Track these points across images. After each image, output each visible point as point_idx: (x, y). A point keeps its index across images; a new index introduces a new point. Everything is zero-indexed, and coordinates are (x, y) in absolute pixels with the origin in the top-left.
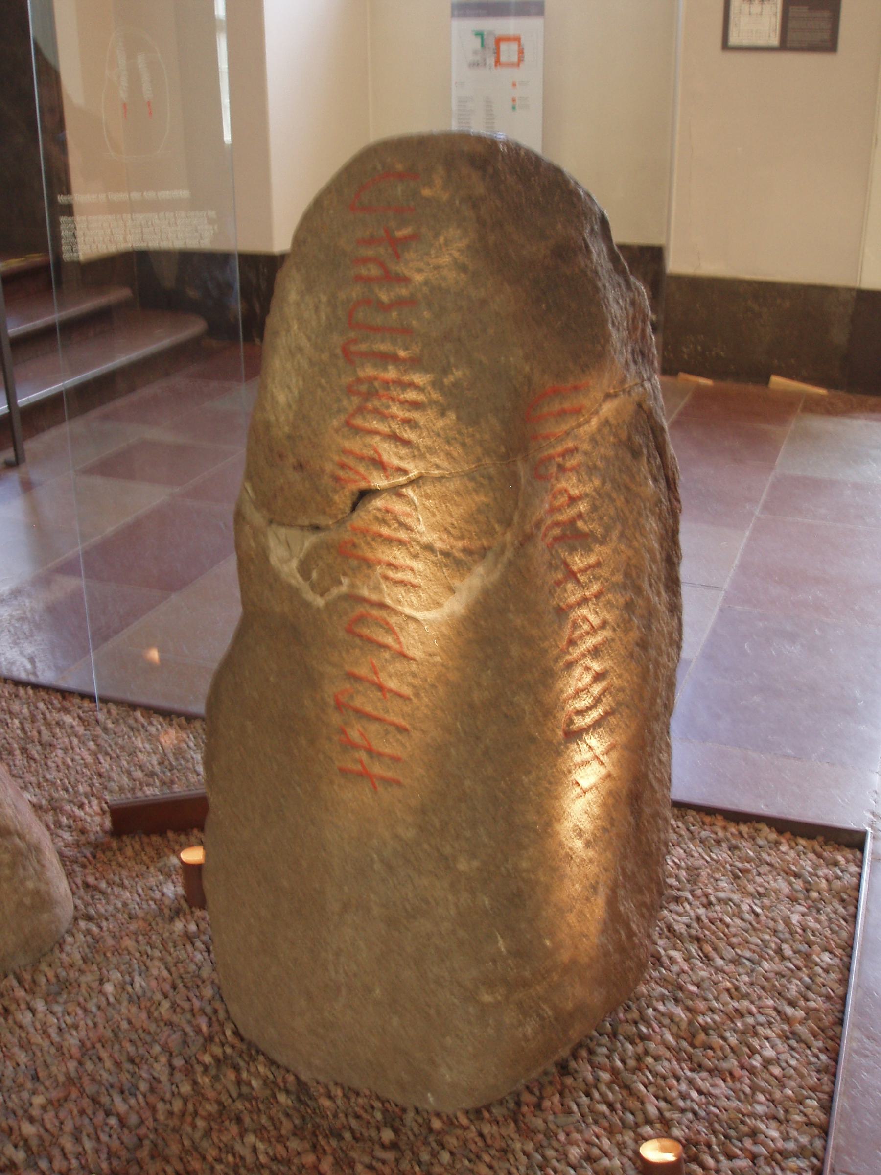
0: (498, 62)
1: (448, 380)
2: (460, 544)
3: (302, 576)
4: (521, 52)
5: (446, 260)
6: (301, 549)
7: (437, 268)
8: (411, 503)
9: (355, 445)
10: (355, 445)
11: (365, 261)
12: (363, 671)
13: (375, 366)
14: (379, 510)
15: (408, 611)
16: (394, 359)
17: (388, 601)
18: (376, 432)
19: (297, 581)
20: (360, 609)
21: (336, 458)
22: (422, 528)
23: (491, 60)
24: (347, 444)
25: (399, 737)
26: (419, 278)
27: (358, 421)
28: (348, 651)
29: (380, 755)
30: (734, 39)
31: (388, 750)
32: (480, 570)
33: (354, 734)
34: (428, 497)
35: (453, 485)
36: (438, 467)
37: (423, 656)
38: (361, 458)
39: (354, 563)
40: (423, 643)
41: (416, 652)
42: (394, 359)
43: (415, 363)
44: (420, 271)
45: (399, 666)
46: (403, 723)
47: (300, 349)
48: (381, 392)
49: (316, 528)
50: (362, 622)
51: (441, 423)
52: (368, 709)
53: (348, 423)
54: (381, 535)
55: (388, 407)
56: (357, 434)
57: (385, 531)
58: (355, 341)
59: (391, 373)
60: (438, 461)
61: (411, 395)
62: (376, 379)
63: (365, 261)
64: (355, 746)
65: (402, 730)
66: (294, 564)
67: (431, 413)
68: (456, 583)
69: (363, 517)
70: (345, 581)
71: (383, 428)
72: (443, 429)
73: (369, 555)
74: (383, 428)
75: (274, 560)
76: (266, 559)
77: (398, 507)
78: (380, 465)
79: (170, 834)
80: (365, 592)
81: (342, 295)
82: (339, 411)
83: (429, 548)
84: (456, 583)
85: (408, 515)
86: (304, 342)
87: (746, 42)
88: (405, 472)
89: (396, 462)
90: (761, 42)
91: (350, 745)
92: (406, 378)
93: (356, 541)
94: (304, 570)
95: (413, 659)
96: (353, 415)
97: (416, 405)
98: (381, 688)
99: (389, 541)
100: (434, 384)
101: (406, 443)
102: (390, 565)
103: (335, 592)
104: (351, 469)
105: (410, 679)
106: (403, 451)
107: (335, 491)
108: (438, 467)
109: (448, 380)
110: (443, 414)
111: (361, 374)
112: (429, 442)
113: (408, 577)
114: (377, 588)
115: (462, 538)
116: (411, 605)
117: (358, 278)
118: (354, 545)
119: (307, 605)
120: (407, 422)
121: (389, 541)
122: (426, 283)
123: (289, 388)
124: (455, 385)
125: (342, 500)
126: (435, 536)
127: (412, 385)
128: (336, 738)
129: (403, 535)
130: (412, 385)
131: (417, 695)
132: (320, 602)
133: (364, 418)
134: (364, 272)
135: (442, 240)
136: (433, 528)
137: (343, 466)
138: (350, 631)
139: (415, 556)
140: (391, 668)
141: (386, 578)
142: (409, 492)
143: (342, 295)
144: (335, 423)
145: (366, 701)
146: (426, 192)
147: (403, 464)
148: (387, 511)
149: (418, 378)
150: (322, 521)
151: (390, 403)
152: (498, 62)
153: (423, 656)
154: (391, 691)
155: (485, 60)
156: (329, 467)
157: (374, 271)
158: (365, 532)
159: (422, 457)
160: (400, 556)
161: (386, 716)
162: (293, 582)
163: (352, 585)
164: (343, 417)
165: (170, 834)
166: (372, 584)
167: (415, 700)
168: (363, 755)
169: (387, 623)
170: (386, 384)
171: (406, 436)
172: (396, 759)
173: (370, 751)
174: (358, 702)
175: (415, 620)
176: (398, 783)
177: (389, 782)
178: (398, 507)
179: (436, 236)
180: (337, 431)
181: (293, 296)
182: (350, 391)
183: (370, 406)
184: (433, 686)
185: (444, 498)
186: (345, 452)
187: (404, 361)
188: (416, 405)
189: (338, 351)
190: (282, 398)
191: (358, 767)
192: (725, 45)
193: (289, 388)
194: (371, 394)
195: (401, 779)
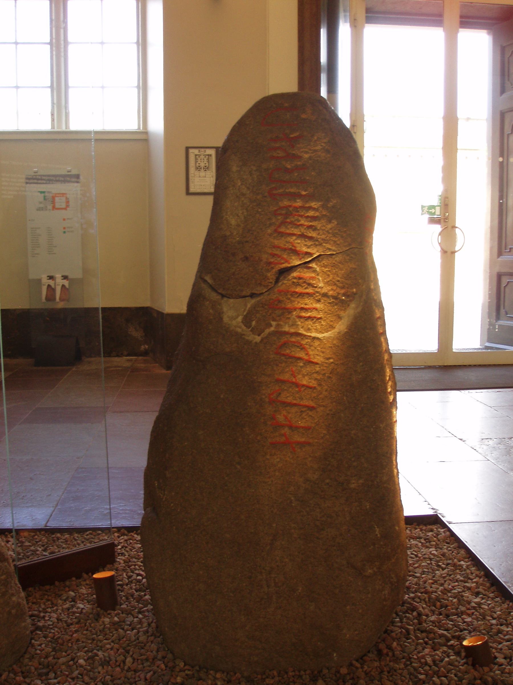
0: (54, 208)
1: (330, 204)
2: (343, 291)
3: (245, 326)
4: (68, 202)
5: (319, 148)
6: (245, 310)
7: (315, 151)
8: (315, 271)
9: (281, 242)
10: (281, 242)
11: (276, 149)
12: (286, 377)
13: (289, 200)
14: (295, 278)
15: (313, 335)
16: (300, 196)
17: (302, 331)
18: (293, 235)
19: (242, 329)
20: (284, 339)
21: (270, 251)
22: (321, 285)
23: (50, 207)
24: (276, 242)
25: (310, 413)
26: (306, 156)
27: (283, 229)
28: (277, 365)
29: (297, 428)
30: (192, 190)
31: (301, 424)
32: (353, 305)
33: (280, 418)
34: (325, 266)
35: (338, 258)
36: (330, 249)
37: (322, 359)
38: (285, 250)
39: (279, 312)
40: (323, 352)
41: (319, 359)
42: (300, 196)
43: (311, 197)
44: (306, 153)
45: (309, 369)
46: (312, 404)
47: (243, 195)
48: (294, 213)
49: (252, 295)
50: (285, 347)
51: (329, 226)
52: (289, 400)
53: (276, 231)
54: (297, 293)
55: (299, 221)
56: (282, 236)
57: (299, 289)
58: (275, 188)
59: (299, 203)
60: (330, 247)
61: (311, 213)
62: (290, 206)
63: (276, 149)
64: (283, 426)
65: (312, 408)
66: (240, 319)
67: (323, 221)
68: (342, 313)
69: (285, 283)
70: (274, 323)
71: (296, 231)
72: (331, 229)
73: (289, 306)
74: (296, 231)
75: (226, 319)
76: (221, 319)
77: (307, 274)
78: (295, 252)
79: (57, 583)
80: (286, 329)
81: (264, 166)
82: (271, 225)
83: (325, 295)
84: (342, 313)
85: (313, 278)
86: (245, 190)
87: (199, 191)
88: (311, 254)
89: (305, 249)
90: (206, 191)
91: (279, 426)
92: (307, 205)
93: (281, 298)
94: (247, 321)
95: (317, 364)
96: (279, 226)
97: (314, 218)
98: (297, 385)
99: (302, 295)
100: (323, 206)
101: (311, 238)
102: (302, 309)
103: (267, 331)
104: (279, 256)
105: (315, 375)
106: (309, 243)
107: (268, 271)
108: (330, 249)
109: (330, 204)
110: (330, 221)
111: (281, 204)
112: (323, 237)
113: (314, 314)
114: (294, 324)
115: (342, 288)
116: (317, 330)
117: (273, 157)
118: (280, 301)
119: (249, 342)
120: (310, 227)
121: (302, 295)
122: (310, 158)
123: (238, 216)
124: (333, 207)
125: (271, 275)
126: (329, 288)
127: (310, 208)
128: (269, 423)
129: (310, 290)
130: (310, 208)
131: (320, 385)
132: (258, 339)
133: (286, 227)
134: (275, 154)
135: (316, 138)
136: (327, 283)
137: (273, 255)
138: (277, 353)
139: (319, 301)
140: (304, 371)
141: (300, 317)
142: (313, 265)
143: (264, 166)
144: (269, 231)
145: (286, 397)
146: (304, 116)
147: (309, 250)
148: (300, 278)
149: (313, 204)
150: (258, 290)
151: (300, 218)
152: (54, 208)
153: (322, 359)
154: (303, 385)
155: (46, 207)
156: (265, 257)
157: (281, 154)
158: (286, 292)
159: (321, 245)
160: (309, 303)
161: (301, 403)
162: (239, 330)
163: (278, 325)
164: (273, 228)
165: (57, 583)
166: (290, 323)
167: (319, 388)
168: (286, 430)
169: (301, 345)
170: (296, 208)
171: (310, 235)
172: (308, 428)
173: (291, 427)
174: (283, 398)
175: (318, 339)
176: (309, 444)
177: (302, 444)
178: (307, 274)
179: (313, 136)
180: (270, 235)
181: (235, 169)
182: (275, 214)
183: (288, 220)
184: (329, 377)
185: (334, 266)
186: (275, 247)
187: (305, 195)
188: (314, 218)
189: (266, 194)
190: (233, 222)
191: (283, 439)
192: (188, 193)
193: (238, 216)
194: (287, 215)
195: (311, 441)
